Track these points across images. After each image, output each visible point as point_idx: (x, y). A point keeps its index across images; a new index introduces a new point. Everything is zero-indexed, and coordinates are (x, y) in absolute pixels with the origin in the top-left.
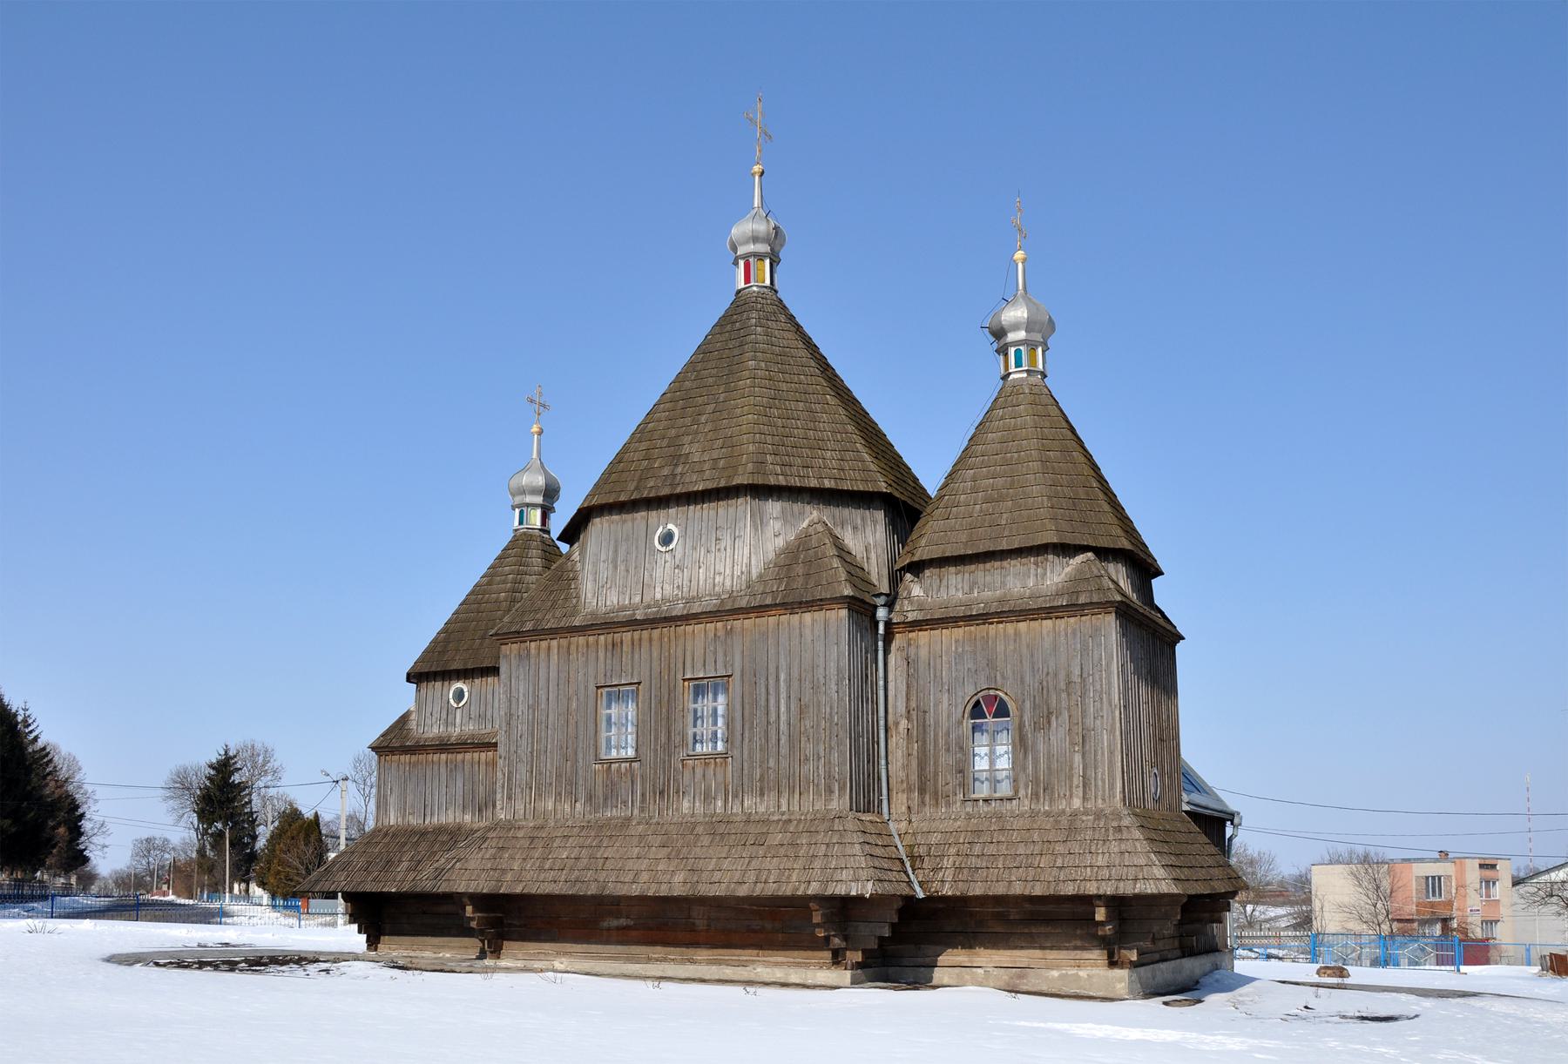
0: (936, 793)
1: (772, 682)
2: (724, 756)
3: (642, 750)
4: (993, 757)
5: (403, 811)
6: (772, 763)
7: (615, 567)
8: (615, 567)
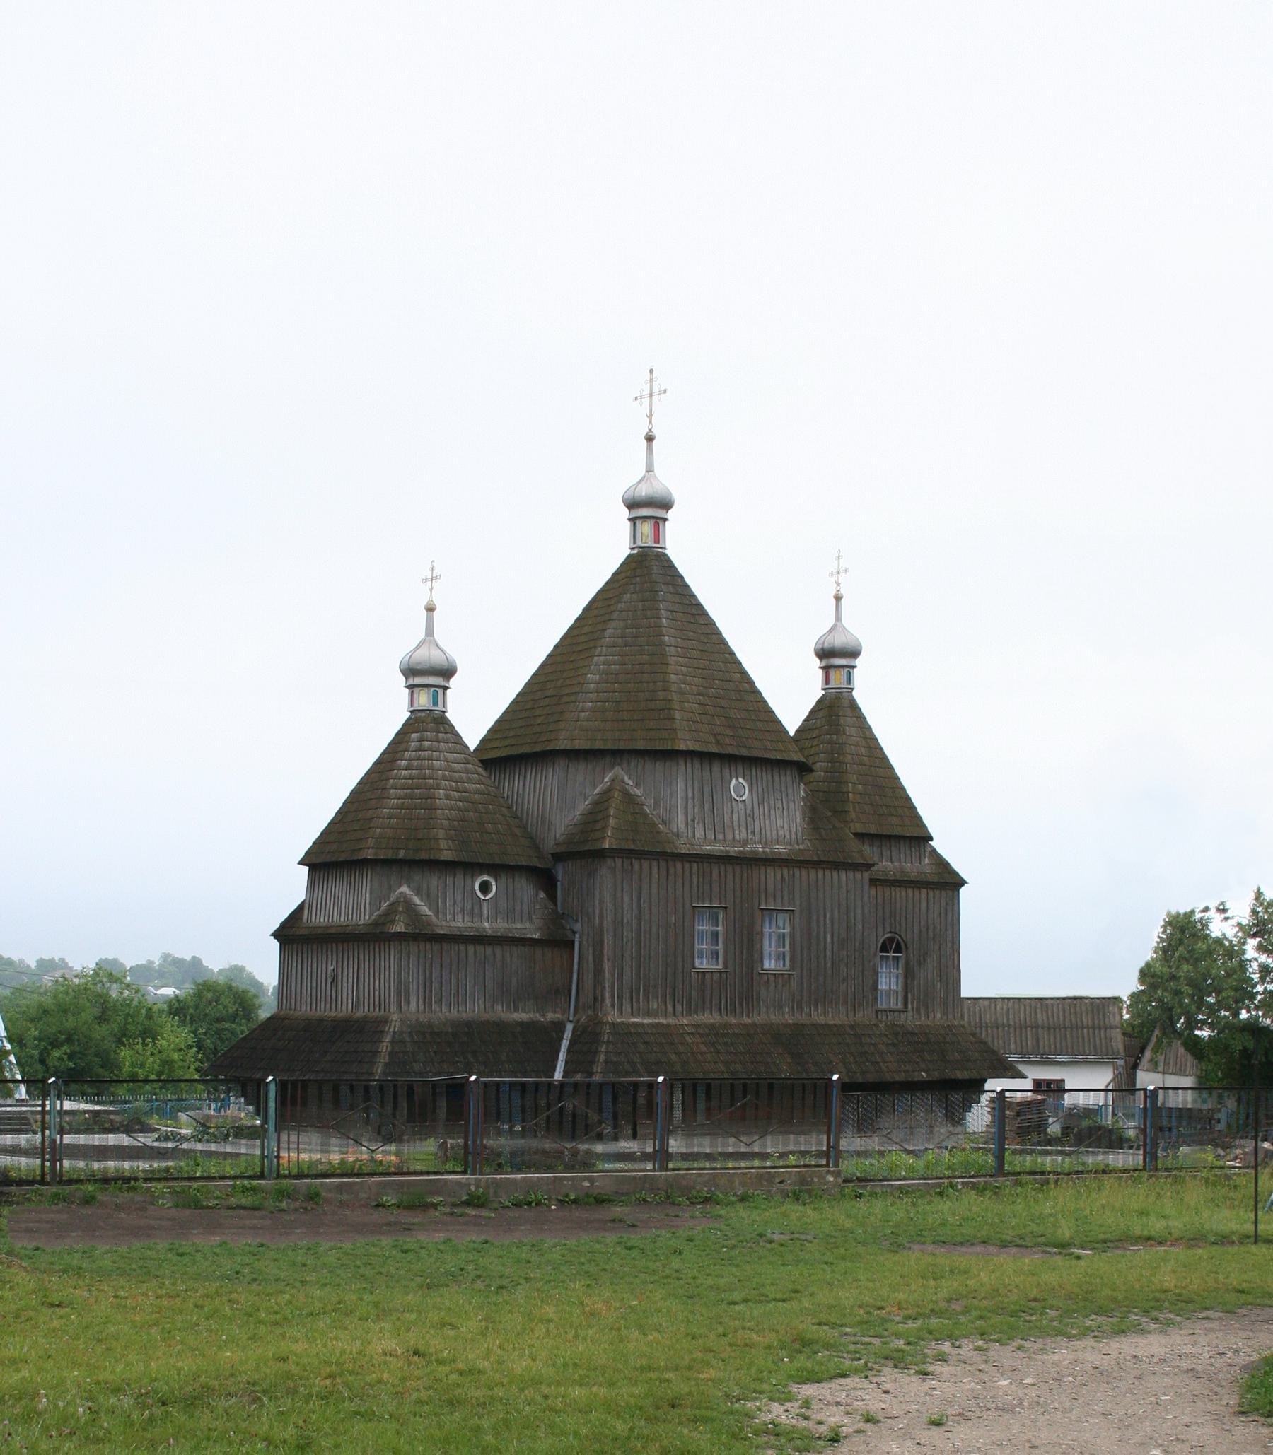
4: (888, 980)
5: (427, 1000)
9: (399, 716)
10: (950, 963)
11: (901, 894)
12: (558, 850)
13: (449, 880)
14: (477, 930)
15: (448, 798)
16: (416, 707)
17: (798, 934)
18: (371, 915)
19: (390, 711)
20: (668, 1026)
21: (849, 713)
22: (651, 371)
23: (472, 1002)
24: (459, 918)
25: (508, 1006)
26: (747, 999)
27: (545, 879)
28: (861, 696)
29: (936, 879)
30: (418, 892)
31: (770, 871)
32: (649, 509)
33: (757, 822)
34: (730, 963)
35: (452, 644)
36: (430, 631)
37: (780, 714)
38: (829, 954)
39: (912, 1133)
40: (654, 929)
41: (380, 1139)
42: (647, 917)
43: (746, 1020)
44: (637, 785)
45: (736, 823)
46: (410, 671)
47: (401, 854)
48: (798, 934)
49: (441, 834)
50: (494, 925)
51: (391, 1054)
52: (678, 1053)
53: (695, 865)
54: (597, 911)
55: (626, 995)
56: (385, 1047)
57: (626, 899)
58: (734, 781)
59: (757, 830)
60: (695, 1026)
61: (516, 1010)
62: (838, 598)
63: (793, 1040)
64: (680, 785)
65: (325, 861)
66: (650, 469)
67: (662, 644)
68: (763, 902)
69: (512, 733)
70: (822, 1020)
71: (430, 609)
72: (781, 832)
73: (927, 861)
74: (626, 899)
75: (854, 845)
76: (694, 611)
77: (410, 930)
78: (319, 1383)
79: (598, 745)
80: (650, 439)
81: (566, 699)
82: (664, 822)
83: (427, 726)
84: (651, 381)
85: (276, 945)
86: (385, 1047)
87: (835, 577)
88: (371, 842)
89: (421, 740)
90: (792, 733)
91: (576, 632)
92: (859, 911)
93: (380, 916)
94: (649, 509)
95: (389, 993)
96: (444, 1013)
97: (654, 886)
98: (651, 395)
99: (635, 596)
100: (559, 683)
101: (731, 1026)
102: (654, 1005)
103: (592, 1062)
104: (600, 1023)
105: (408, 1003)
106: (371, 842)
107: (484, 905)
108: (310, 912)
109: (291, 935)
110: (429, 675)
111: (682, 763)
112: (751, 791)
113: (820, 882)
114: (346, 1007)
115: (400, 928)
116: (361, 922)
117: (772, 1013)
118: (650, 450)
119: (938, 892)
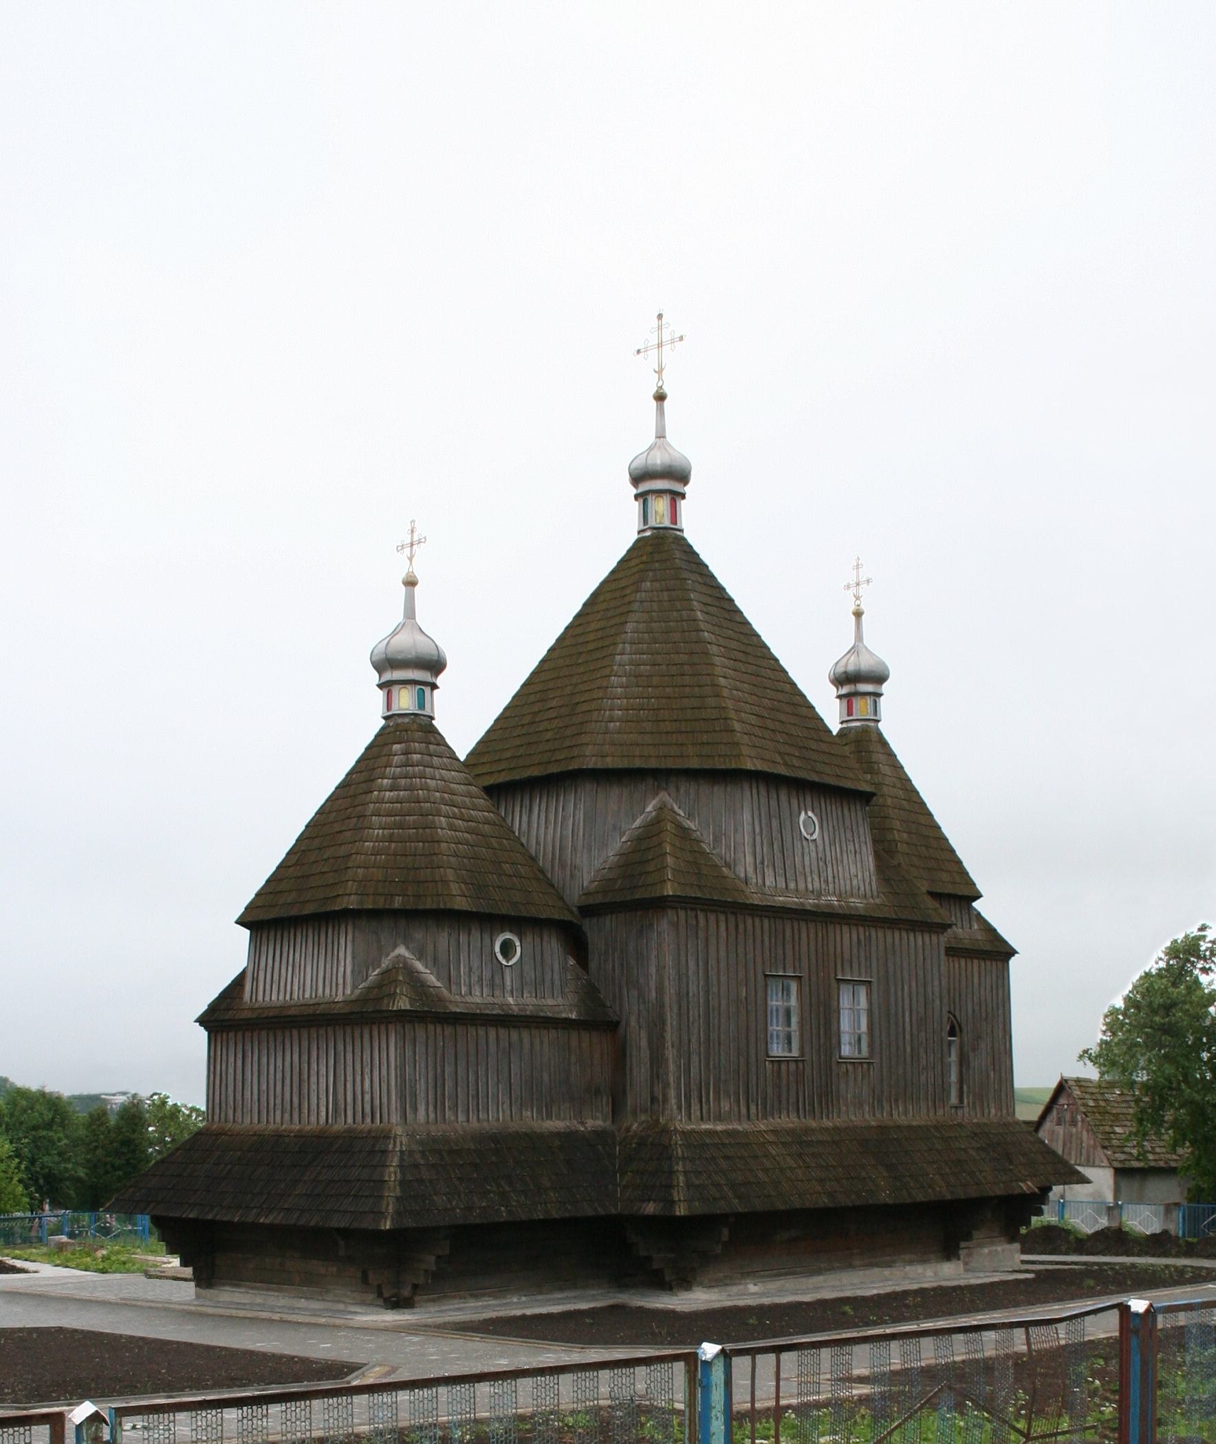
5: (438, 1104)
9: (374, 724)
10: (1002, 1048)
12: (591, 901)
13: (463, 938)
14: (501, 1006)
15: (452, 828)
16: (395, 710)
17: (876, 1011)
18: (354, 987)
19: (361, 717)
20: (745, 1134)
21: (880, 749)
22: (660, 316)
23: (495, 1103)
24: (477, 991)
25: (540, 1111)
26: (826, 1096)
27: (574, 939)
28: (889, 728)
29: (988, 948)
30: (421, 956)
32: (661, 481)
33: (830, 869)
34: (807, 1049)
35: (440, 629)
36: (410, 612)
38: (908, 1037)
40: (723, 1007)
41: (380, 1302)
42: (715, 989)
43: (827, 1123)
44: (690, 816)
45: (808, 869)
46: (385, 663)
47: (398, 903)
48: (876, 1011)
49: (450, 874)
50: (520, 1001)
51: (402, 1183)
52: (766, 1170)
53: (766, 921)
54: (653, 984)
55: (695, 1095)
56: (392, 1174)
57: (692, 964)
58: (803, 814)
59: (830, 879)
60: (774, 1132)
61: (549, 1117)
62: (858, 614)
63: (882, 1144)
64: (747, 816)
65: (274, 917)
66: (661, 435)
67: (699, 641)
68: (839, 972)
69: (508, 754)
70: (902, 1120)
71: (410, 583)
72: (855, 882)
73: (976, 927)
74: (692, 964)
75: (931, 903)
76: (726, 606)
77: (417, 1007)
79: (638, 763)
80: (660, 397)
81: (585, 707)
82: (728, 865)
83: (408, 735)
84: (660, 328)
85: (203, 1034)
86: (392, 1174)
87: (853, 590)
88: (351, 887)
89: (406, 753)
91: (579, 630)
92: (936, 983)
93: (369, 988)
94: (661, 481)
95: (368, 1091)
96: (462, 1122)
97: (722, 948)
98: (660, 345)
99: (657, 585)
100: (568, 690)
101: (813, 1130)
102: (725, 1106)
103: (669, 1187)
104: (665, 1131)
105: (415, 1110)
106: (351, 887)
107: (506, 973)
108: (254, 990)
110: (411, 668)
111: (746, 786)
112: (821, 827)
113: (897, 948)
114: (317, 1115)
115: (403, 1004)
116: (340, 998)
117: (854, 1112)
118: (661, 412)
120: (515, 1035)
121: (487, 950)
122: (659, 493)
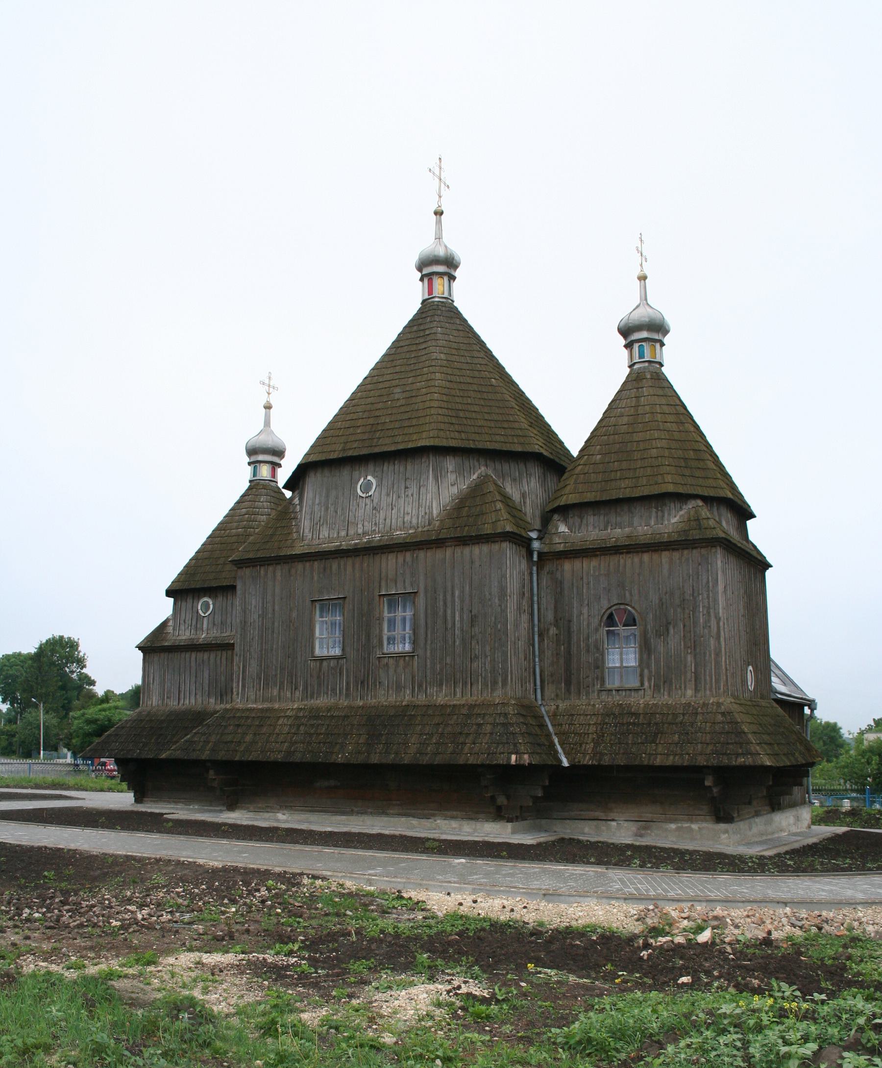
0: (579, 683)
1: (449, 597)
2: (411, 656)
3: (348, 649)
4: (622, 657)
6: (448, 660)
7: (327, 509)
8: (327, 509)
11: (630, 563)
29: (675, 537)
31: (392, 557)
32: (438, 267)
36: (267, 423)
37: (567, 445)
39: (646, 828)
58: (362, 480)
78: (465, 711)
85: (140, 654)
90: (575, 453)
94: (438, 267)
96: (173, 704)
109: (154, 647)
118: (439, 223)
119: (686, 552)
120: (206, 655)
121: (195, 609)
122: (441, 275)
